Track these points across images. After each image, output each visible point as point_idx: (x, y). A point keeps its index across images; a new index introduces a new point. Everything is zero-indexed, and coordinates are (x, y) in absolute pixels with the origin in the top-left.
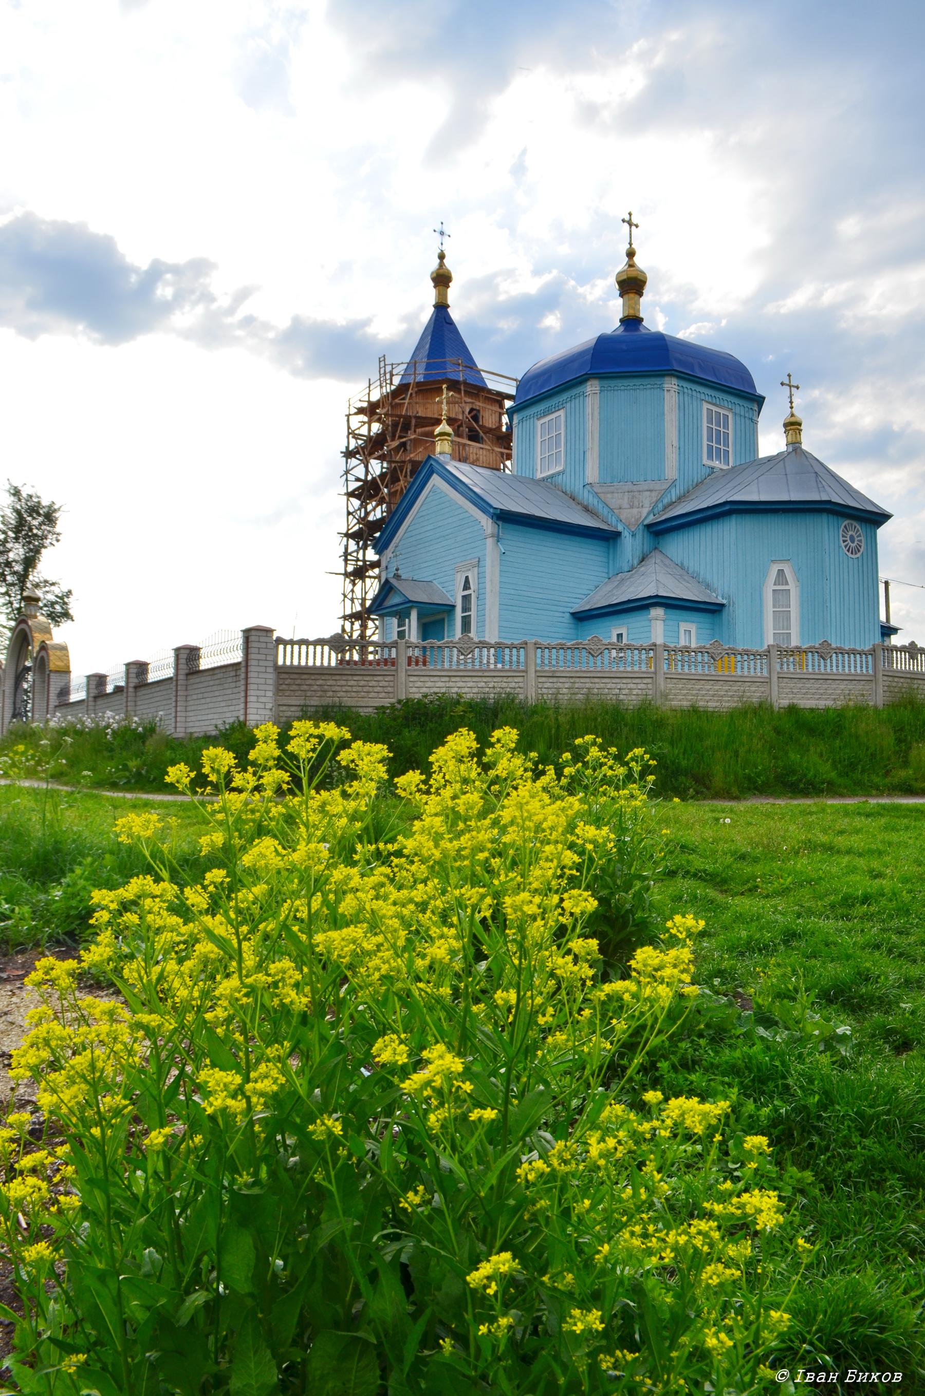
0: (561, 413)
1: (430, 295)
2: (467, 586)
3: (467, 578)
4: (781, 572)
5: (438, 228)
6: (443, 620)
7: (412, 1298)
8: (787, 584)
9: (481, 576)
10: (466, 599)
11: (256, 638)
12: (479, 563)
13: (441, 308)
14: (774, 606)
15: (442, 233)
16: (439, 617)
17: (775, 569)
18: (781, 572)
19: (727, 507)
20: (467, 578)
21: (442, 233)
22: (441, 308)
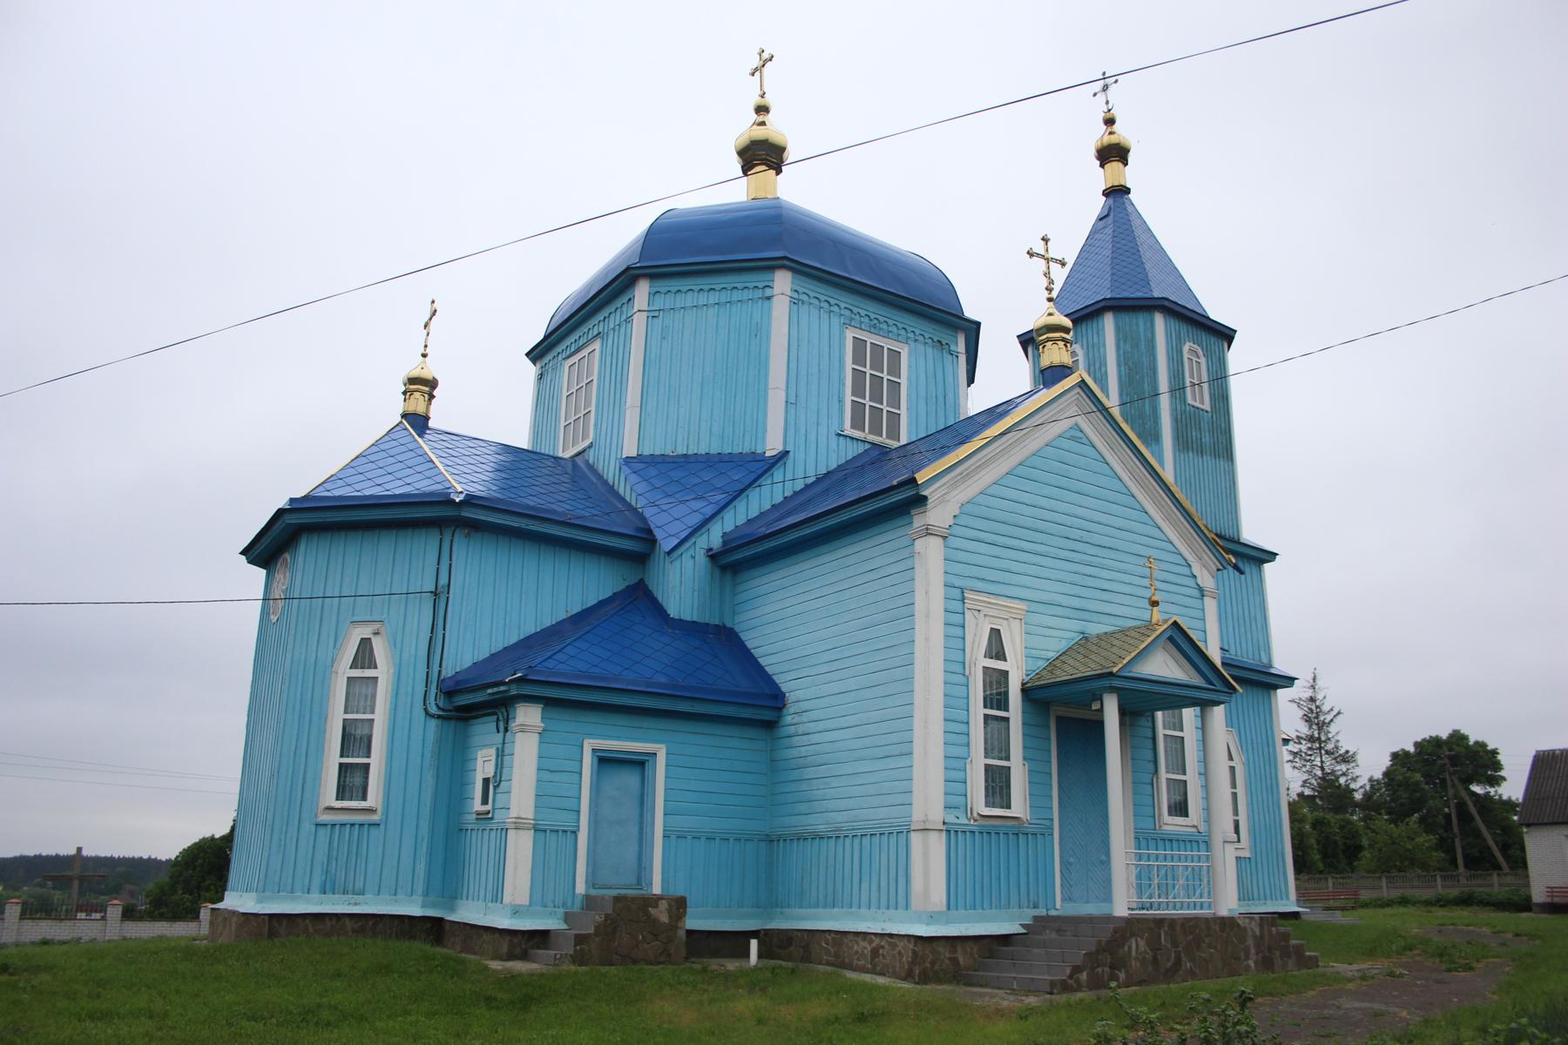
1: (1098, 178)
13: (1117, 193)
18: (365, 644)
22: (1117, 193)
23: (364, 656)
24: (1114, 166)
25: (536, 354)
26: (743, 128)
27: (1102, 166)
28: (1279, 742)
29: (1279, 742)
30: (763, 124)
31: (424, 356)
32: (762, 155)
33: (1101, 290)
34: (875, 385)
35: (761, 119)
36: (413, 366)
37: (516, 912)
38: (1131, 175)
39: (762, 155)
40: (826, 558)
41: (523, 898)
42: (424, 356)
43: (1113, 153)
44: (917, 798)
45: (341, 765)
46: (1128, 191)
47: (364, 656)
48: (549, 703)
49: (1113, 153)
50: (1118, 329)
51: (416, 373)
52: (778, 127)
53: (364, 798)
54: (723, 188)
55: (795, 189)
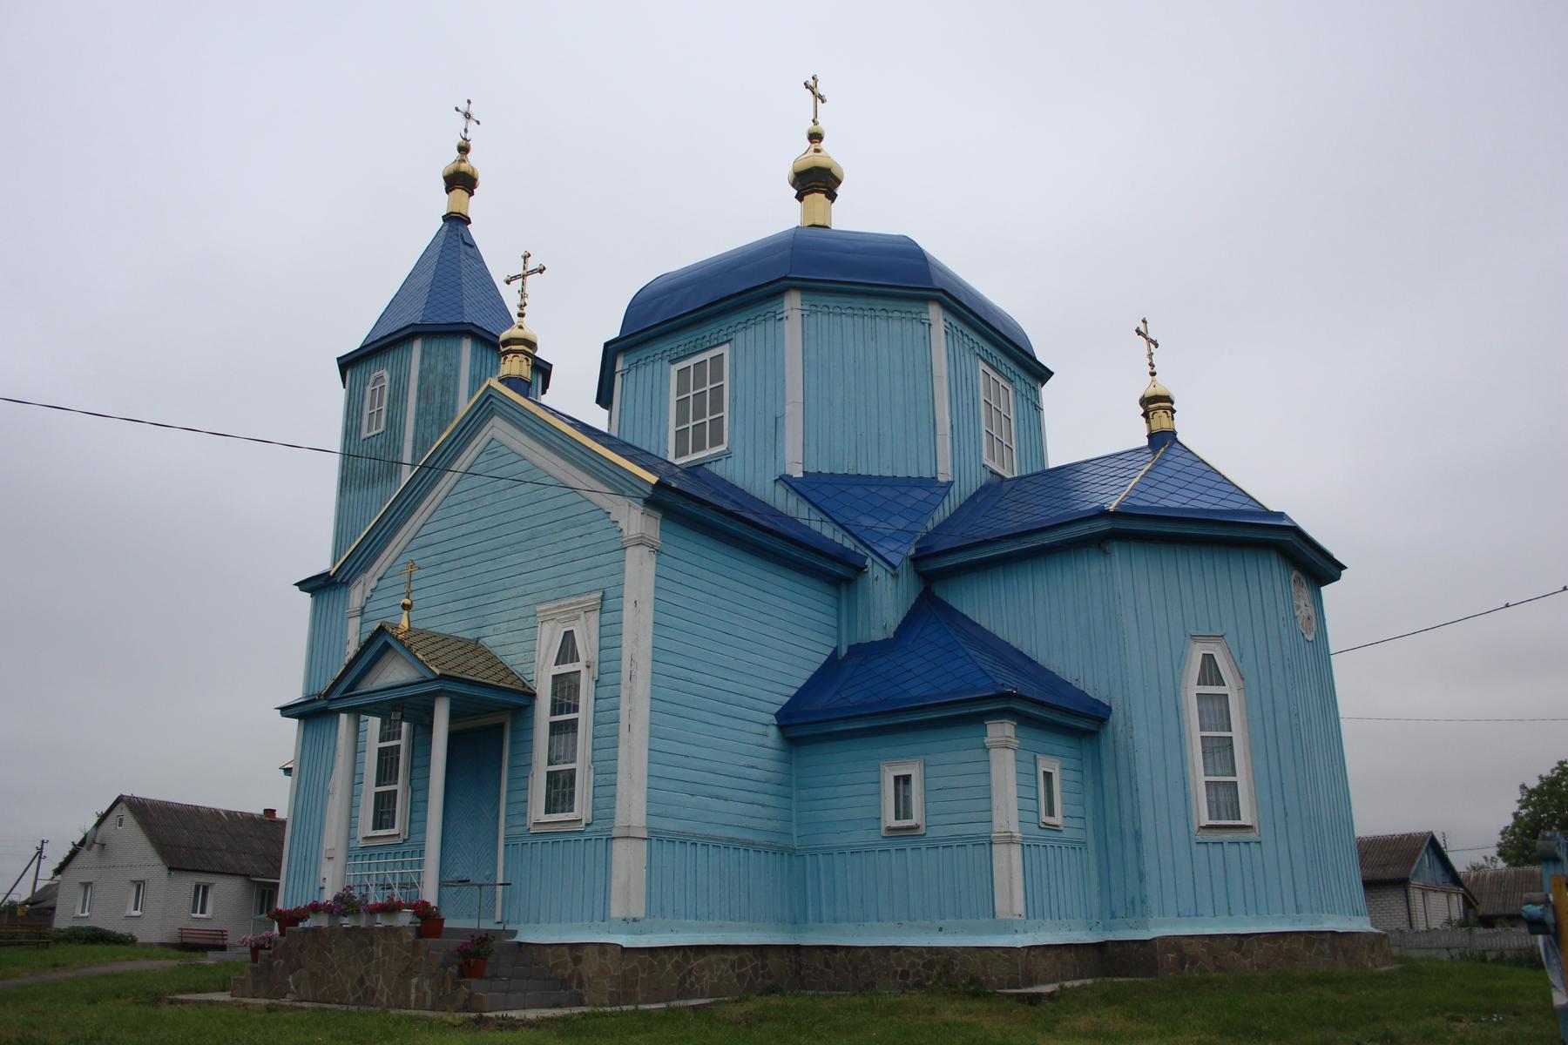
0: (725, 350)
1: (441, 202)
2: (567, 650)
3: (569, 635)
4: (1208, 659)
5: (463, 107)
6: (500, 728)
7: (129, 834)
8: (1221, 682)
9: (610, 636)
10: (565, 689)
11: (1541, 777)
12: (607, 605)
13: (456, 221)
14: (1202, 729)
15: (468, 116)
16: (490, 720)
17: (1197, 652)
18: (1208, 659)
19: (1102, 526)
20: (569, 635)
21: (468, 116)
22: (456, 221)
23: (1210, 672)
24: (459, 193)
25: (347, 364)
26: (797, 151)
27: (800, 197)
28: (295, 772)
29: (295, 772)
30: (817, 151)
31: (1153, 374)
32: (816, 181)
33: (414, 315)
34: (701, 409)
35: (818, 146)
36: (1144, 387)
37: (630, 922)
38: (476, 207)
39: (816, 181)
40: (769, 576)
41: (638, 909)
42: (1153, 374)
43: (461, 181)
44: (997, 818)
45: (549, 774)
46: (468, 221)
47: (1210, 672)
48: (1023, 720)
49: (461, 181)
50: (423, 351)
51: (1151, 392)
52: (833, 153)
53: (572, 810)
54: (779, 214)
55: (851, 214)
